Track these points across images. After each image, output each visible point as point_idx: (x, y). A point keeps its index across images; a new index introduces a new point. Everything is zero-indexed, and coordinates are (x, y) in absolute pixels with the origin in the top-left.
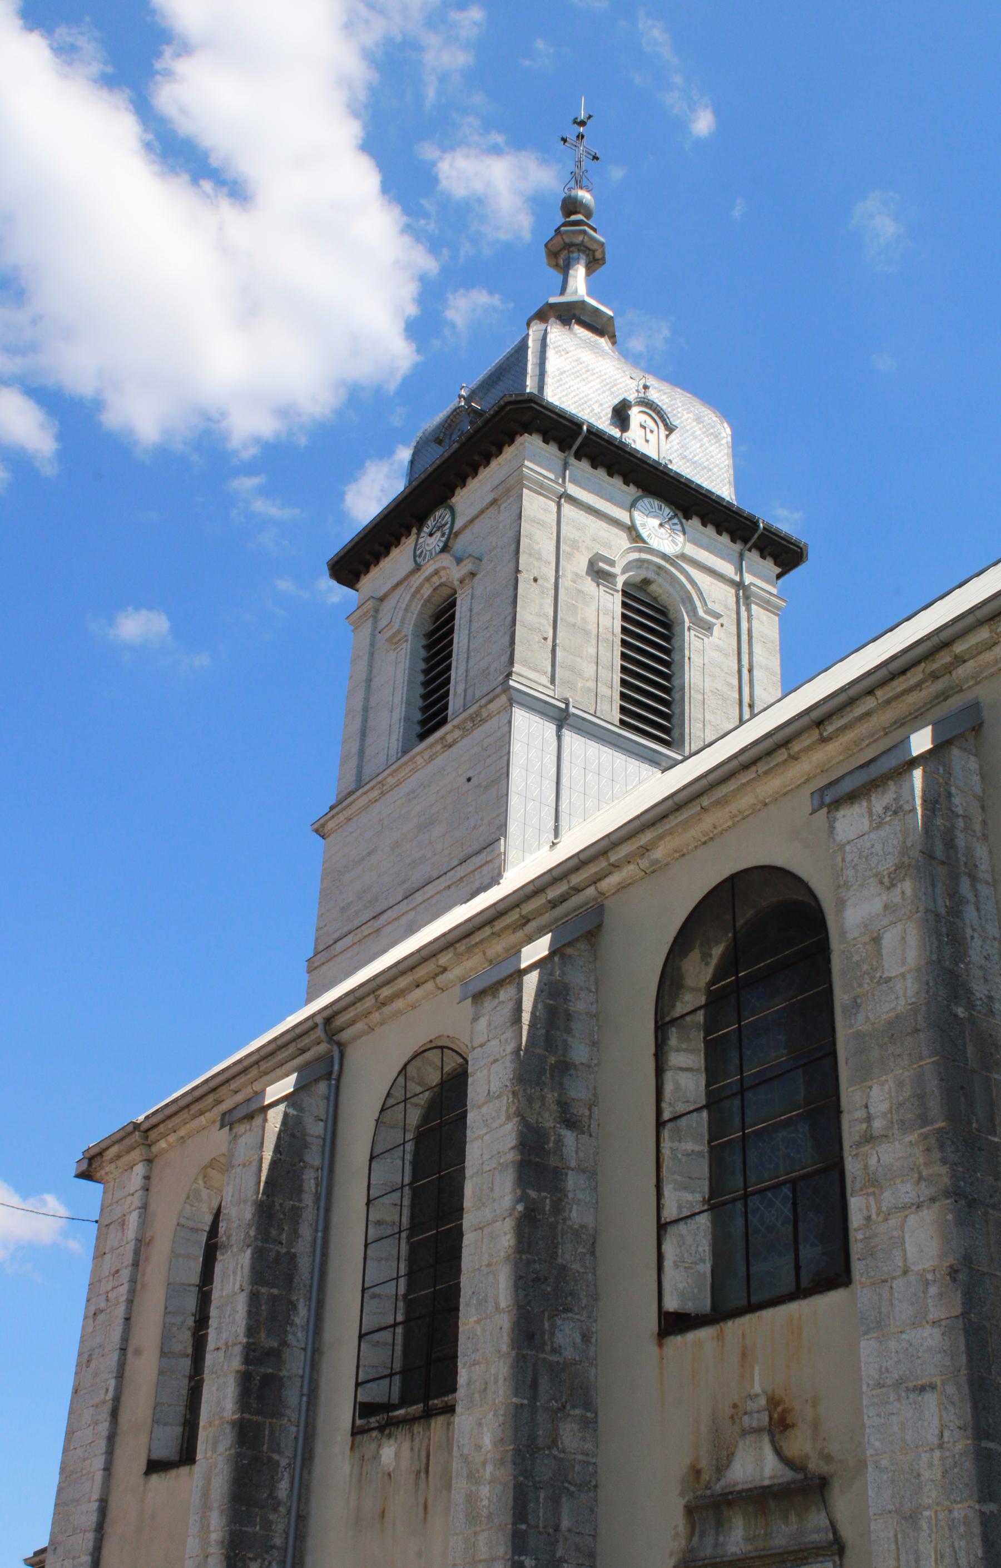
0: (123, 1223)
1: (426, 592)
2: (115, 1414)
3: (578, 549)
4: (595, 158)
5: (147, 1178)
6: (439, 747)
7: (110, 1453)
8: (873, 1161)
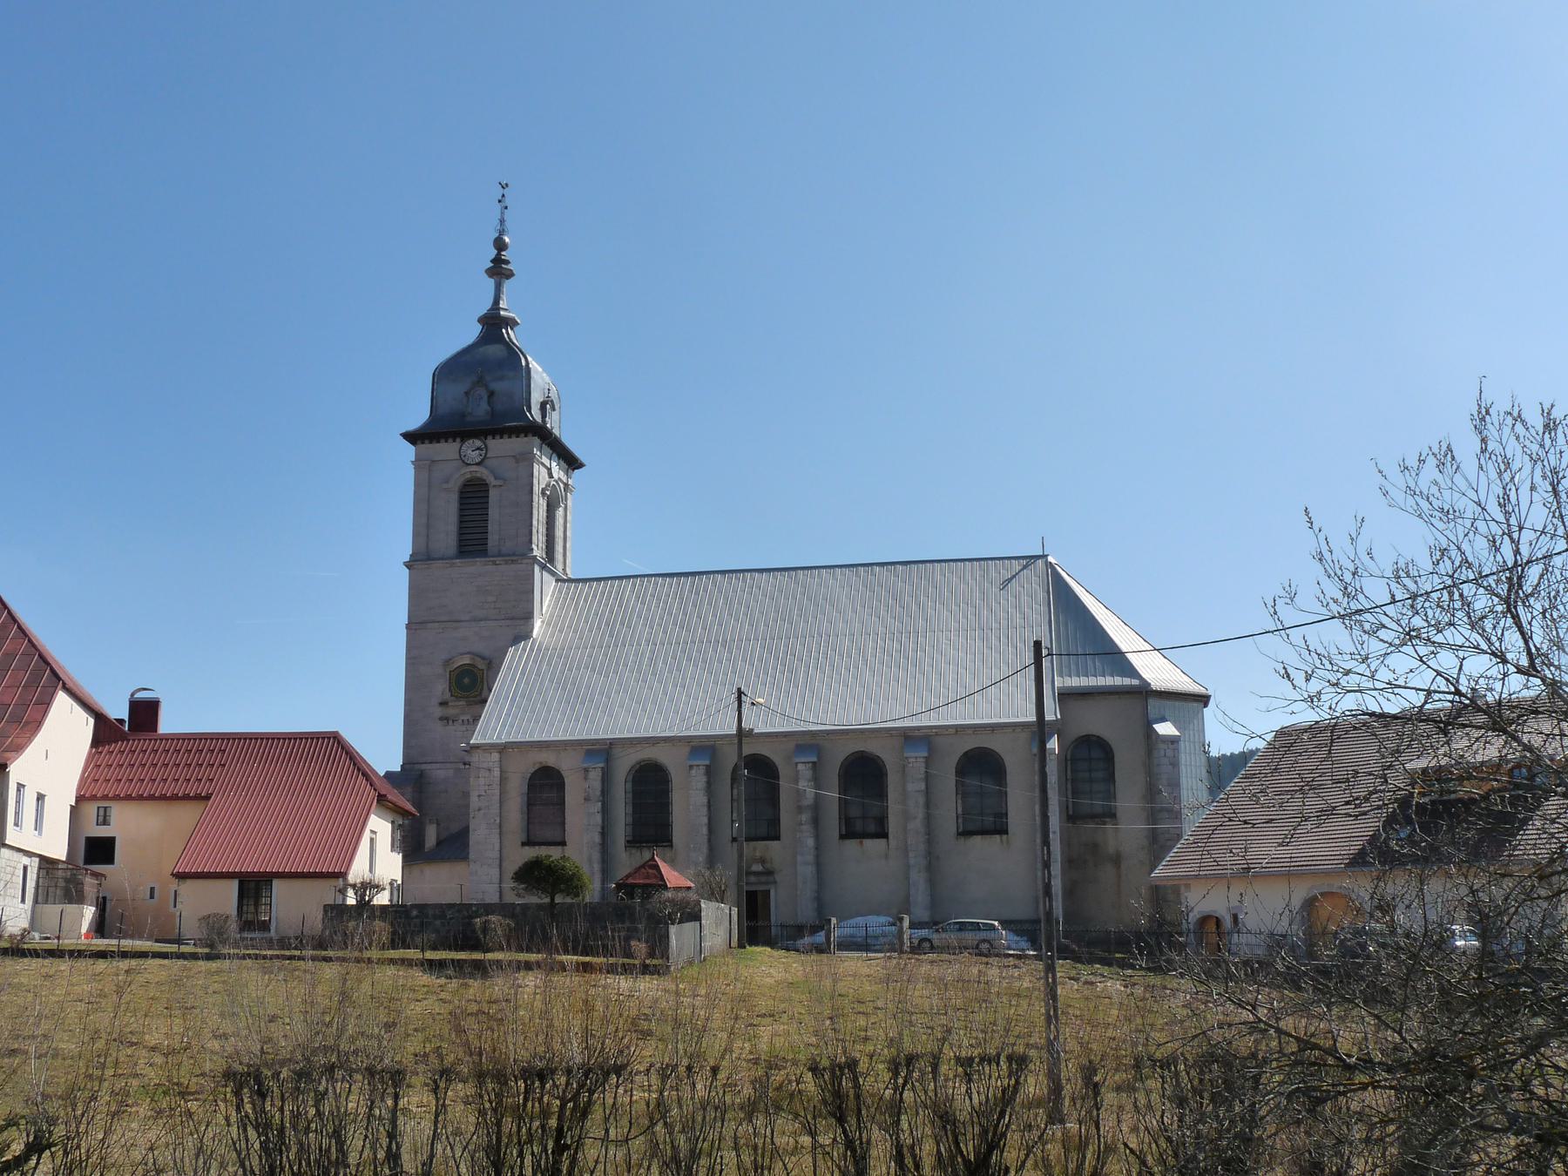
1: (469, 476)
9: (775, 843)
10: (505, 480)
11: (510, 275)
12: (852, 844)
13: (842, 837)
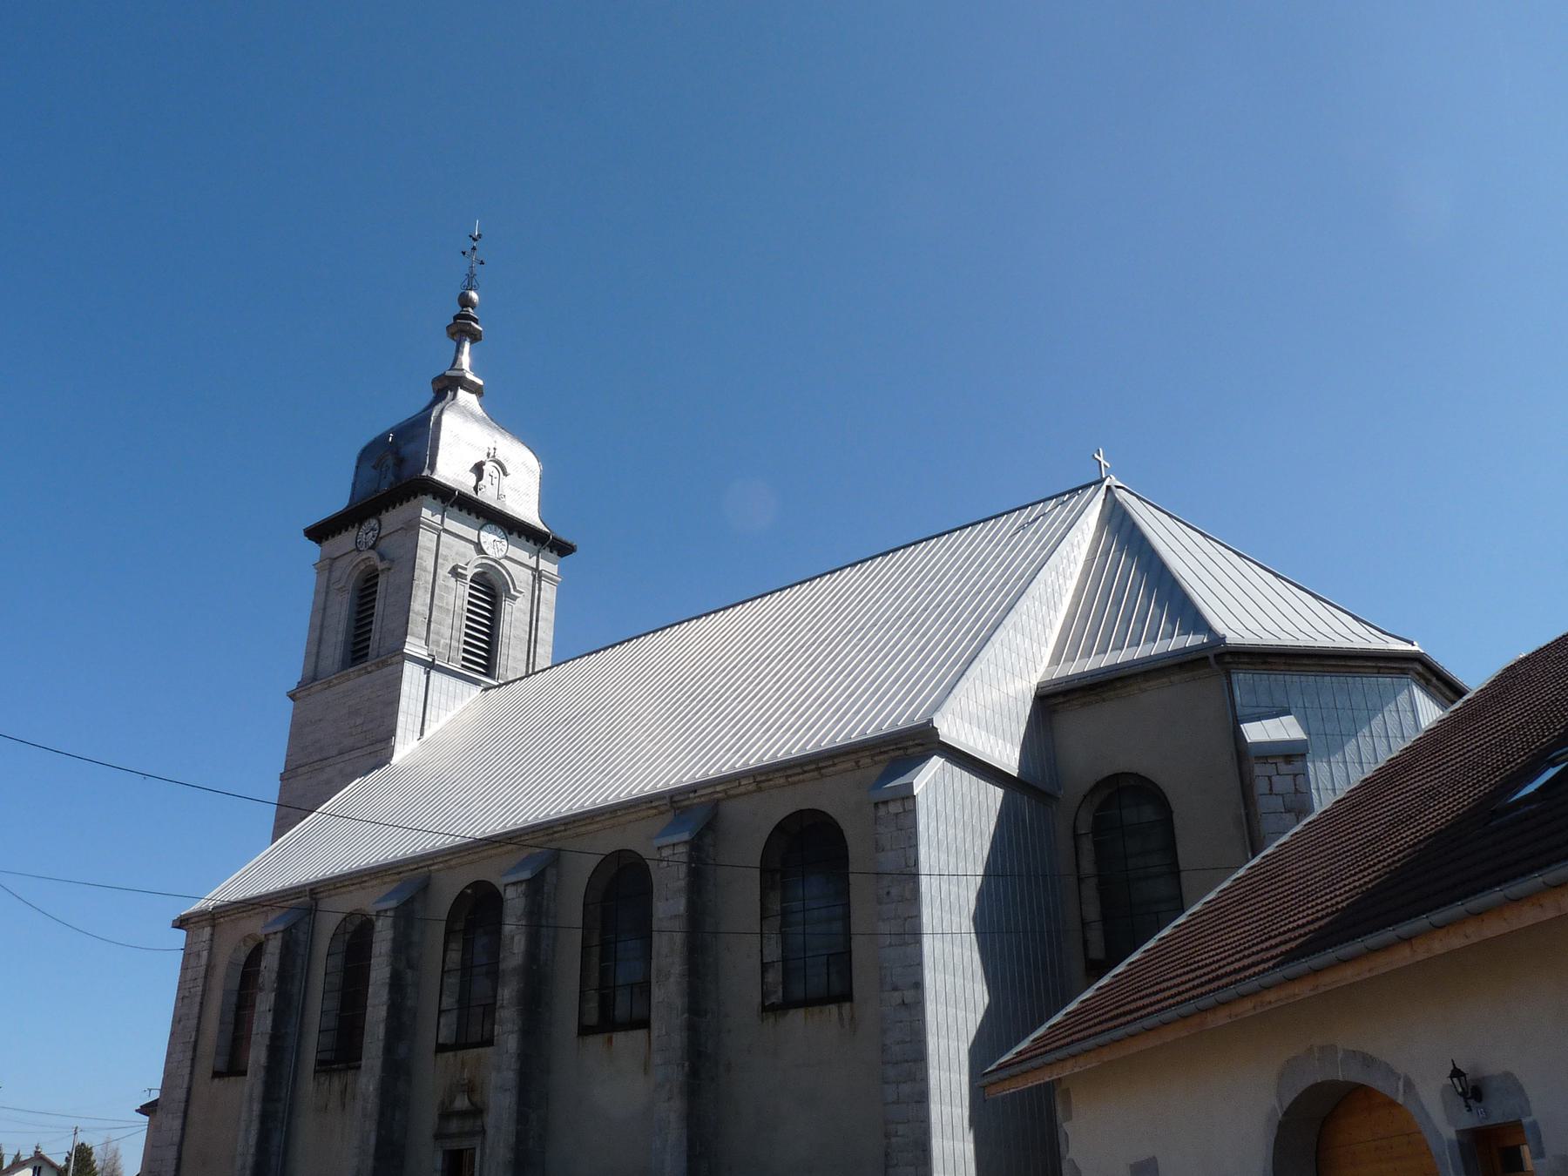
0: (199, 955)
2: (195, 1049)
3: (447, 560)
4: (482, 263)
5: (212, 935)
7: (192, 1066)
8: (502, 1014)
9: (489, 1050)
10: (392, 561)
12: (596, 1042)
13: (584, 1030)
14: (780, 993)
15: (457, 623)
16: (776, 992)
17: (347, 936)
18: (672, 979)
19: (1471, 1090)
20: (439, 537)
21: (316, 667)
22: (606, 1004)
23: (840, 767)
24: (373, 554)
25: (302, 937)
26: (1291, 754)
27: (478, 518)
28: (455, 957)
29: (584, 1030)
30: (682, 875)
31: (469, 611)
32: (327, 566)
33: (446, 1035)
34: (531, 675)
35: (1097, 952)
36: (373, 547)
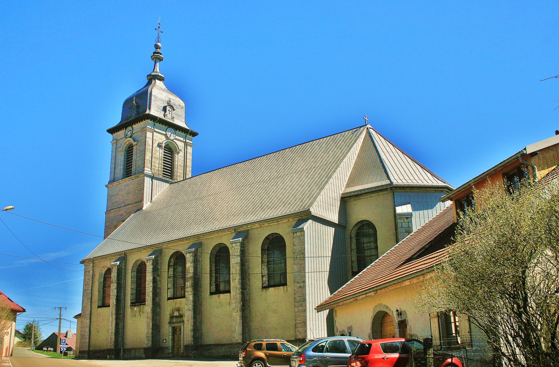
1: (127, 143)
4: (162, 32)
6: (131, 179)
11: (161, 60)
12: (215, 297)
14: (267, 283)
15: (160, 162)
16: (266, 283)
17: (137, 267)
18: (236, 280)
19: (400, 314)
20: (153, 133)
21: (114, 177)
22: (217, 286)
23: (284, 221)
24: (130, 139)
25: (123, 267)
26: (408, 216)
27: (165, 126)
28: (171, 273)
29: (211, 294)
30: (239, 252)
31: (164, 157)
32: (116, 142)
33: (170, 294)
34: (185, 180)
35: (355, 270)
36: (130, 137)
